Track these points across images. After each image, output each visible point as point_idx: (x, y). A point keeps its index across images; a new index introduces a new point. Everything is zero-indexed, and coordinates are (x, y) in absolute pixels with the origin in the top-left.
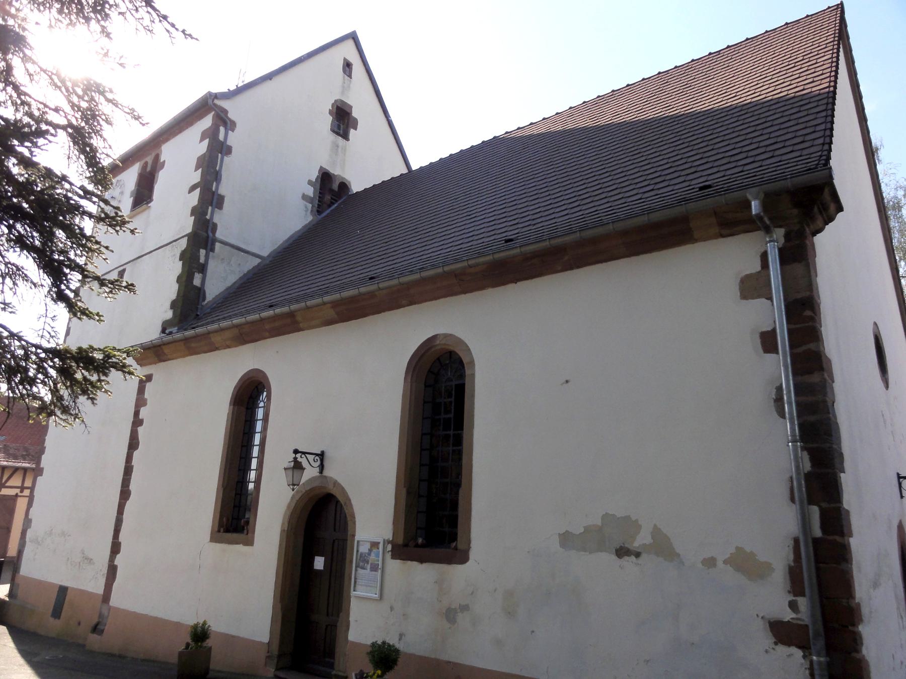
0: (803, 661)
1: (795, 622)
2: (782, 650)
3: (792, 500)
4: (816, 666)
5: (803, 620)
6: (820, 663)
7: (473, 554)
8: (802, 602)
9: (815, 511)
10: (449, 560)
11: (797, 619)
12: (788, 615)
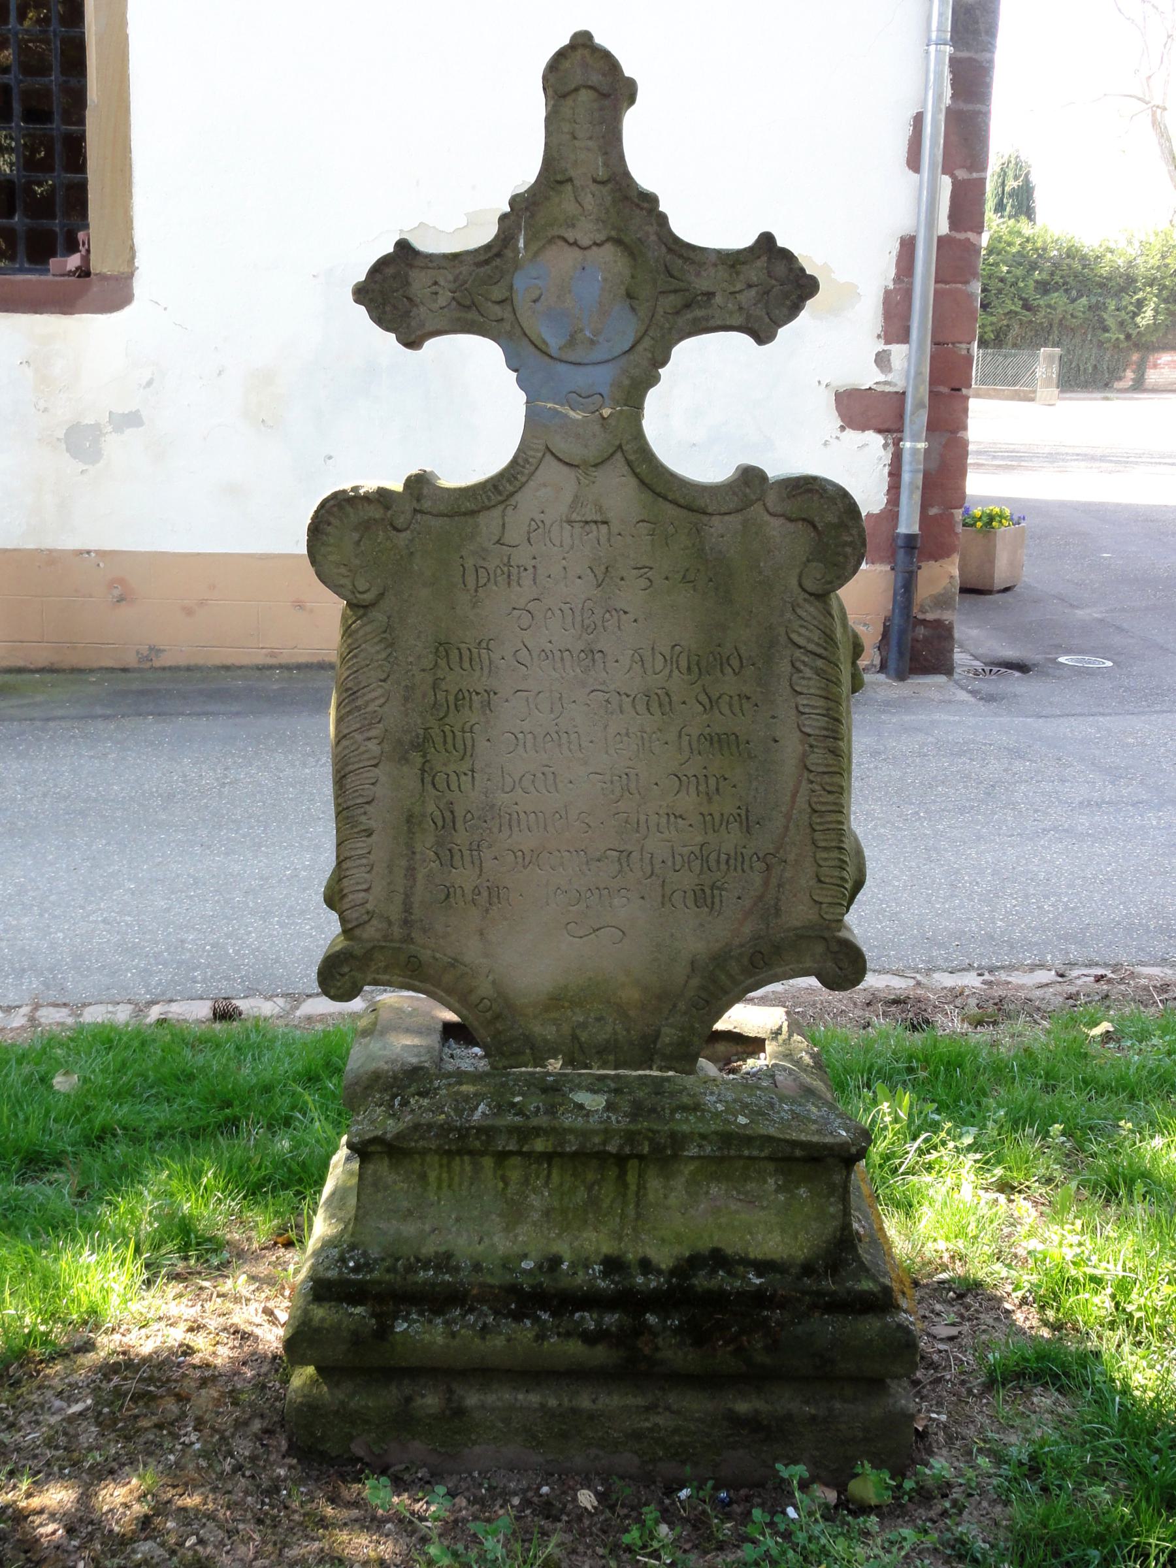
0: (882, 452)
1: (880, 388)
2: (853, 437)
3: (914, 162)
4: (906, 457)
5: (895, 385)
6: (915, 451)
7: (140, 286)
8: (898, 352)
9: (946, 183)
10: (63, 303)
11: (886, 383)
12: (869, 377)
